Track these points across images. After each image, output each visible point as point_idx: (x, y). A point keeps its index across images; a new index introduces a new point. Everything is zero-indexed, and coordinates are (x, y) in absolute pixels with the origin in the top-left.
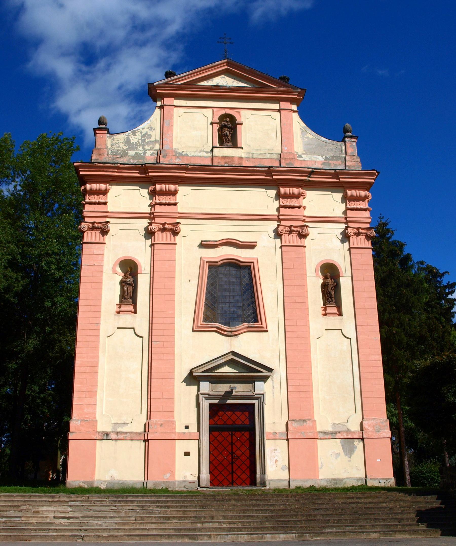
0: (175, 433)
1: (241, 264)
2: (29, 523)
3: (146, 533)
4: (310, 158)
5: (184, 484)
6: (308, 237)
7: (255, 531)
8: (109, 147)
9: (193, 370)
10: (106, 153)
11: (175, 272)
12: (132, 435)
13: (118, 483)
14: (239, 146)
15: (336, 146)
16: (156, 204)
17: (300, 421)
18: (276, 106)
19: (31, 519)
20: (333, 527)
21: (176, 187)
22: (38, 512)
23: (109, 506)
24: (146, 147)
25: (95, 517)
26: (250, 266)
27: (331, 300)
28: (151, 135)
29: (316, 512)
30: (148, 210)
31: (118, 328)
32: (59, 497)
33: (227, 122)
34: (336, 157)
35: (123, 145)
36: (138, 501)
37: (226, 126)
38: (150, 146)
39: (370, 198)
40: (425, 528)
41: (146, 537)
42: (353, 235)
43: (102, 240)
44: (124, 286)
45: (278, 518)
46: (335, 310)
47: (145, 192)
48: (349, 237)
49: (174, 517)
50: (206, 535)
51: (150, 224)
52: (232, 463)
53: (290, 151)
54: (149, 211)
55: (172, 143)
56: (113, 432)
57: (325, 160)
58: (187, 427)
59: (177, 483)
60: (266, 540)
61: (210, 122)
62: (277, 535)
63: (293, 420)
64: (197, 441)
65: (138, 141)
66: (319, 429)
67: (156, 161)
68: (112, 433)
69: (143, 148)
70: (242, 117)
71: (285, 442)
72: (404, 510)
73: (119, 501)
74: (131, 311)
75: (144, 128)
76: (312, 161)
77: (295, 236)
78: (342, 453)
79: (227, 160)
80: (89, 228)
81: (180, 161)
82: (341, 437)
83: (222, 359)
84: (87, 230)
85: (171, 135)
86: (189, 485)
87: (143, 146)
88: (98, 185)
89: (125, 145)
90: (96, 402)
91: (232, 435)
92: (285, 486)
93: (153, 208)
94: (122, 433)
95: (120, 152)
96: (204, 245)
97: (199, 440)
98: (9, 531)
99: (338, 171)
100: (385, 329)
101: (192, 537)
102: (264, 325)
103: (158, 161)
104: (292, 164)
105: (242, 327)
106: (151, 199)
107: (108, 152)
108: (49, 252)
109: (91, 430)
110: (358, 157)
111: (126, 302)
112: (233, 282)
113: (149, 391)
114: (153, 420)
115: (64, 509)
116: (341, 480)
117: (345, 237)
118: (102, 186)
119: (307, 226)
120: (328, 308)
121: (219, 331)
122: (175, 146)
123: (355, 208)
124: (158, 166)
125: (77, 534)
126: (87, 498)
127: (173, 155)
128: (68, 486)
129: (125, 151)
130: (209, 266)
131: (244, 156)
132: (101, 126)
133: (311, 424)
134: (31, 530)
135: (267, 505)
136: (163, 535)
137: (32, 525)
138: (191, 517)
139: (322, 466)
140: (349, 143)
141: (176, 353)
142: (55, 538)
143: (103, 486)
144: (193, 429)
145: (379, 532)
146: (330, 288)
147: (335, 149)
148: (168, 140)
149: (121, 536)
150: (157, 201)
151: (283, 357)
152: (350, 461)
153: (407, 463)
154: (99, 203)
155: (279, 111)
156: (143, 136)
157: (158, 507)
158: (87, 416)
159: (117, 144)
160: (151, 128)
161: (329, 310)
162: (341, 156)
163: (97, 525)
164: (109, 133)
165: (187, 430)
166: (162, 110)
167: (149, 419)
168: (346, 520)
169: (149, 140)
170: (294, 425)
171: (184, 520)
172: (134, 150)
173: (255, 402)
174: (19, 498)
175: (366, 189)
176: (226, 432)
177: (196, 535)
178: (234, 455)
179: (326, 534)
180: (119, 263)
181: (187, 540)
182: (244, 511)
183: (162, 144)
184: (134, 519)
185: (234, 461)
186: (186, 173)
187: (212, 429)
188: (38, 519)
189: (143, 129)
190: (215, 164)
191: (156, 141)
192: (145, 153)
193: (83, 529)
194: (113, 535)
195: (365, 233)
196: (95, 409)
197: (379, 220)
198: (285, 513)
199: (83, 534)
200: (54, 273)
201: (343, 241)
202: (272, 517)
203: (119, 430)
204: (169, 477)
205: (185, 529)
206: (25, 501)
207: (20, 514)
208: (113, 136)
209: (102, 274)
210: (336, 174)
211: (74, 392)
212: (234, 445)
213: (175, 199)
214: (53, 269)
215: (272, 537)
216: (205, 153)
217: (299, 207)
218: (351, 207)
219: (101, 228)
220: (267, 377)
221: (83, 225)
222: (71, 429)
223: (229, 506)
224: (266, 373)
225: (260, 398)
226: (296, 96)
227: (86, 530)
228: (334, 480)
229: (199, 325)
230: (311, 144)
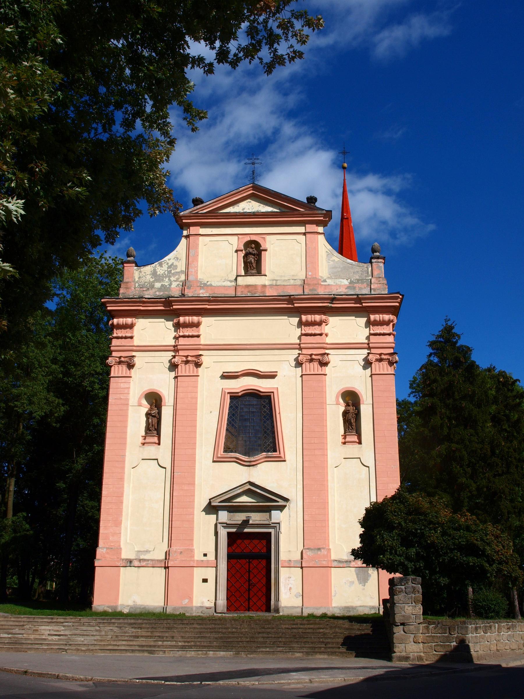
0: (194, 561)
1: (262, 394)
2: (28, 639)
3: (116, 648)
4: (334, 283)
5: (201, 610)
6: (329, 365)
7: (202, 649)
8: (137, 280)
9: (211, 500)
10: (134, 286)
11: (197, 403)
12: (154, 562)
13: (140, 608)
14: (263, 273)
15: (363, 268)
16: (180, 336)
17: (315, 549)
18: (302, 229)
19: (30, 635)
20: (266, 647)
21: (199, 319)
22: (37, 630)
23: (94, 626)
24: (172, 279)
25: (81, 635)
26: (270, 395)
27: (351, 428)
28: (176, 266)
29: (261, 635)
30: (172, 342)
31: (142, 459)
32: (57, 619)
33: (252, 248)
34: (362, 280)
35: (150, 276)
36: (118, 623)
37: (250, 253)
38: (176, 277)
39: (395, 321)
40: (344, 650)
41: (115, 651)
42: (375, 361)
43: (128, 373)
44: (149, 418)
45: (226, 639)
46: (355, 438)
47: (170, 324)
48: (371, 363)
49: (142, 636)
50: (162, 650)
51: (174, 357)
52: (249, 590)
53: (314, 276)
54: (174, 344)
55: (197, 273)
56: (136, 559)
57: (350, 283)
58: (205, 555)
59: (194, 609)
60: (209, 656)
61: (235, 249)
62: (218, 652)
63: (307, 549)
64: (215, 568)
65: (164, 273)
66: (333, 557)
67: (181, 292)
68: (135, 561)
69: (169, 280)
70: (267, 243)
71: (300, 570)
72: (336, 636)
73: (104, 623)
74: (155, 443)
75: (170, 259)
76: (337, 285)
77: (316, 364)
78: (356, 582)
79: (251, 289)
80: (116, 362)
81: (204, 291)
82: (356, 566)
83: (239, 489)
84: (115, 364)
85: (196, 265)
86: (206, 610)
87: (170, 277)
88: (125, 319)
89: (152, 277)
90: (120, 531)
91: (249, 562)
92: (298, 613)
93: (177, 341)
94: (144, 560)
95: (147, 285)
96: (225, 376)
97: (216, 567)
98: (12, 644)
99: (360, 296)
100: (446, 445)
101: (151, 652)
102: (282, 455)
103: (183, 293)
104: (315, 290)
105: (261, 457)
106: (176, 331)
107: (135, 285)
108: (92, 372)
109: (115, 557)
110: (384, 279)
111: (151, 434)
112: (253, 412)
113: (171, 521)
114: (174, 548)
115: (59, 628)
116: (353, 608)
117: (367, 364)
118: (128, 320)
119: (328, 354)
120: (347, 436)
121: (238, 461)
122: (200, 276)
123: (378, 333)
124: (183, 298)
125: (63, 647)
126: (79, 620)
127: (198, 286)
128: (93, 609)
129: (151, 284)
130: (230, 396)
131: (267, 283)
132: (129, 259)
133: (326, 553)
134: (29, 644)
135: (222, 628)
136: (128, 650)
137: (30, 640)
138: (156, 636)
139: (336, 594)
140: (376, 264)
141: (196, 483)
142: (45, 650)
143: (126, 611)
144: (211, 557)
145: (303, 652)
146: (350, 416)
147: (361, 271)
148: (193, 271)
149: (96, 650)
150: (181, 334)
151: (300, 486)
152: (364, 589)
153: (471, 590)
154: (126, 338)
155: (304, 234)
156: (169, 267)
157: (132, 628)
158: (112, 544)
159: (144, 276)
160: (177, 258)
161: (348, 439)
162: (367, 278)
163: (80, 641)
164: (137, 266)
165: (205, 557)
166: (188, 239)
167: (169, 547)
168: (280, 642)
169: (175, 271)
170: (308, 554)
171: (150, 639)
172: (160, 283)
173: (272, 531)
174: (25, 619)
175: (391, 312)
176: (234, 560)
177: (154, 650)
178: (251, 582)
179: (258, 653)
180: (144, 395)
181: (146, 654)
182: (200, 632)
183: (187, 275)
184: (111, 637)
185: (251, 588)
186: (209, 305)
187: (230, 557)
188: (36, 636)
189: (169, 260)
190: (239, 294)
191: (182, 272)
192: (170, 285)
193: (68, 644)
194: (89, 649)
195: (388, 359)
196: (120, 537)
197: (444, 324)
198: (234, 635)
199: (66, 648)
200: (98, 393)
201: (365, 368)
202: (221, 638)
203: (142, 557)
204: (188, 602)
205: (147, 646)
206: (29, 622)
207: (23, 632)
208: (140, 269)
209: (128, 407)
210: (359, 299)
211: (101, 521)
212: (251, 573)
213: (199, 331)
214: (96, 389)
215: (214, 653)
216: (229, 282)
217: (321, 335)
218: (375, 332)
219: (127, 362)
220: (285, 506)
221: (110, 361)
222: (97, 557)
223: (190, 628)
224: (281, 503)
225: (276, 527)
226: (322, 218)
227: (70, 645)
228: (348, 608)
229: (219, 456)
230: (337, 268)
